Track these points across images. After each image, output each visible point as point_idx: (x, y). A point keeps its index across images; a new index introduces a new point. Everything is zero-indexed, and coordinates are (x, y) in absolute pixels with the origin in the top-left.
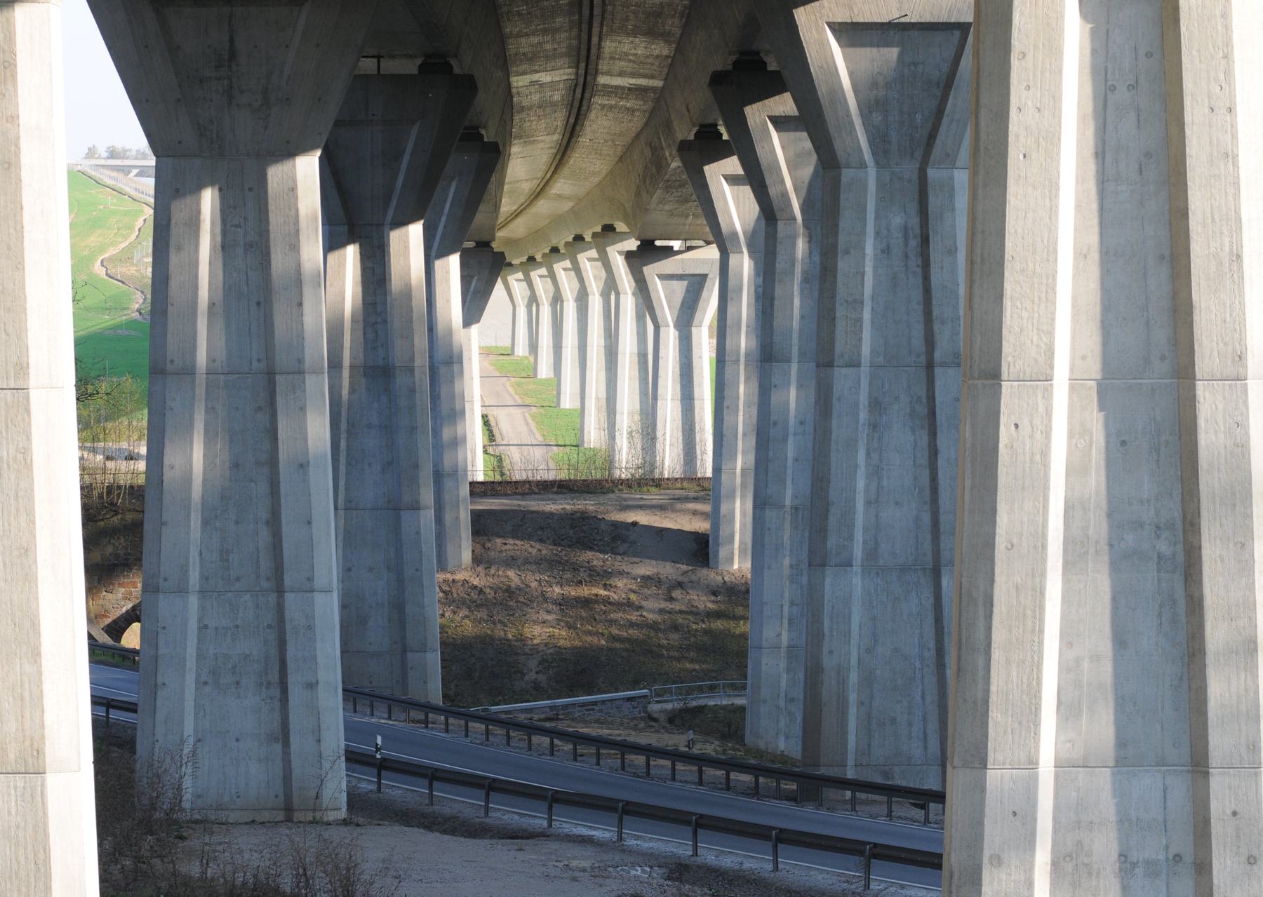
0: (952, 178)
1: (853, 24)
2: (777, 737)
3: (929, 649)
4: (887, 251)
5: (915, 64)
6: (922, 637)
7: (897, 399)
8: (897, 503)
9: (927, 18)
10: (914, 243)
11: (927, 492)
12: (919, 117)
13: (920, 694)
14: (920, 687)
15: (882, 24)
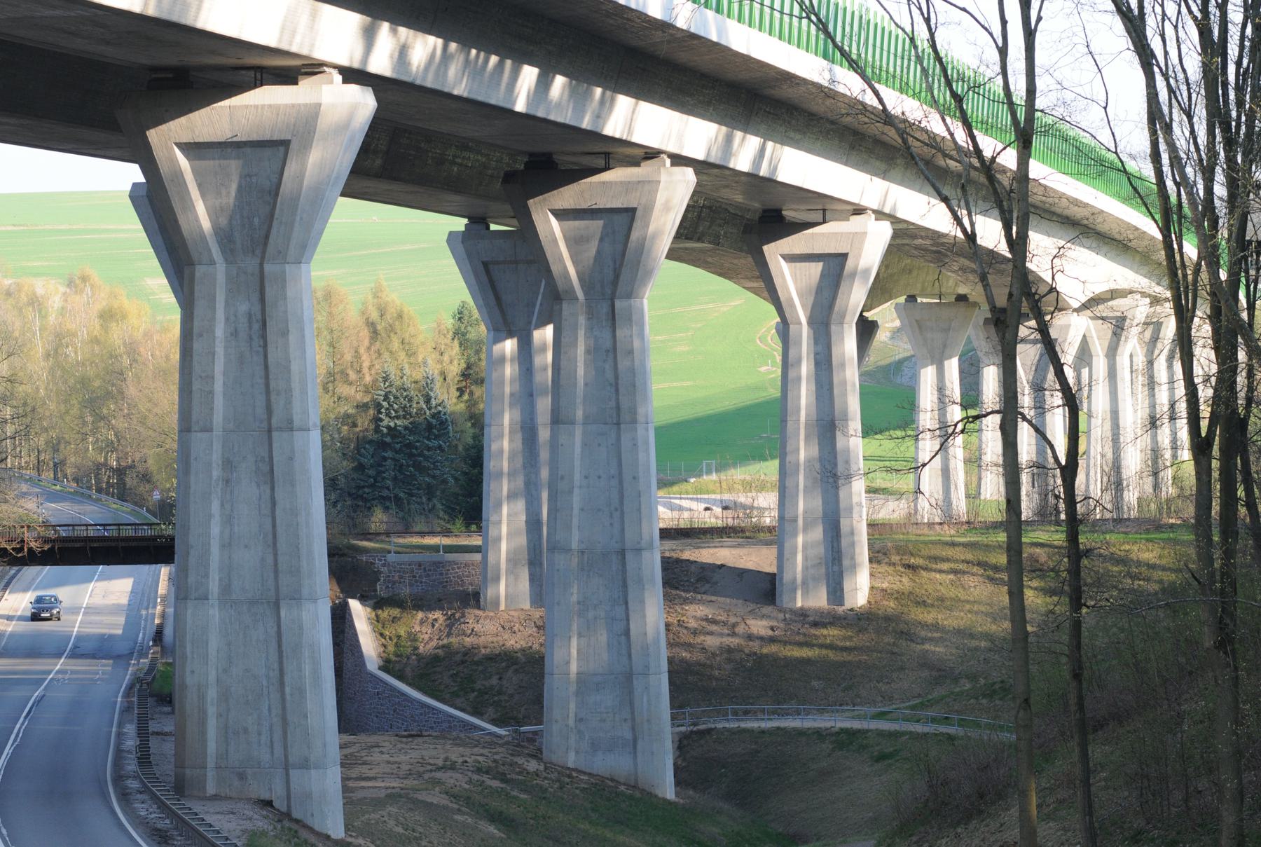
0: (284, 272)
1: (195, 143)
2: (567, 753)
3: (274, 670)
4: (235, 334)
5: (250, 176)
6: (268, 659)
7: (244, 458)
8: (246, 546)
9: (254, 137)
10: (256, 326)
11: (270, 537)
12: (256, 220)
13: (267, 708)
14: (267, 702)
15: (220, 143)
